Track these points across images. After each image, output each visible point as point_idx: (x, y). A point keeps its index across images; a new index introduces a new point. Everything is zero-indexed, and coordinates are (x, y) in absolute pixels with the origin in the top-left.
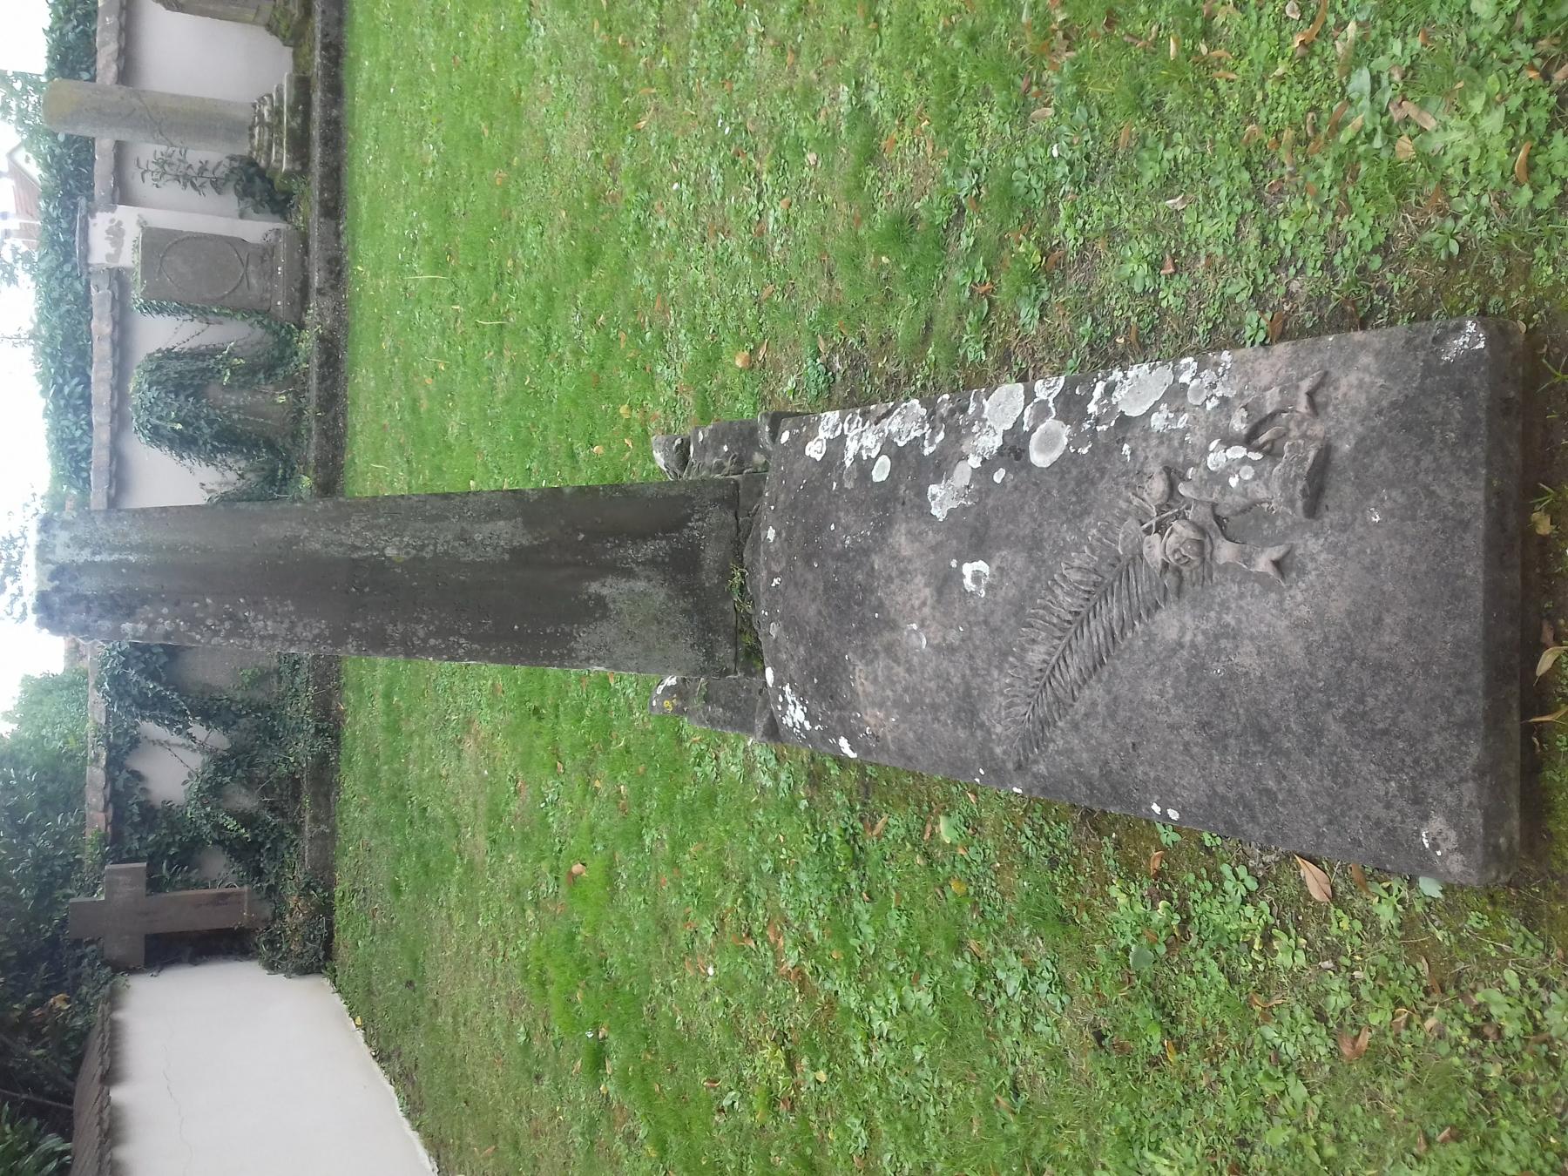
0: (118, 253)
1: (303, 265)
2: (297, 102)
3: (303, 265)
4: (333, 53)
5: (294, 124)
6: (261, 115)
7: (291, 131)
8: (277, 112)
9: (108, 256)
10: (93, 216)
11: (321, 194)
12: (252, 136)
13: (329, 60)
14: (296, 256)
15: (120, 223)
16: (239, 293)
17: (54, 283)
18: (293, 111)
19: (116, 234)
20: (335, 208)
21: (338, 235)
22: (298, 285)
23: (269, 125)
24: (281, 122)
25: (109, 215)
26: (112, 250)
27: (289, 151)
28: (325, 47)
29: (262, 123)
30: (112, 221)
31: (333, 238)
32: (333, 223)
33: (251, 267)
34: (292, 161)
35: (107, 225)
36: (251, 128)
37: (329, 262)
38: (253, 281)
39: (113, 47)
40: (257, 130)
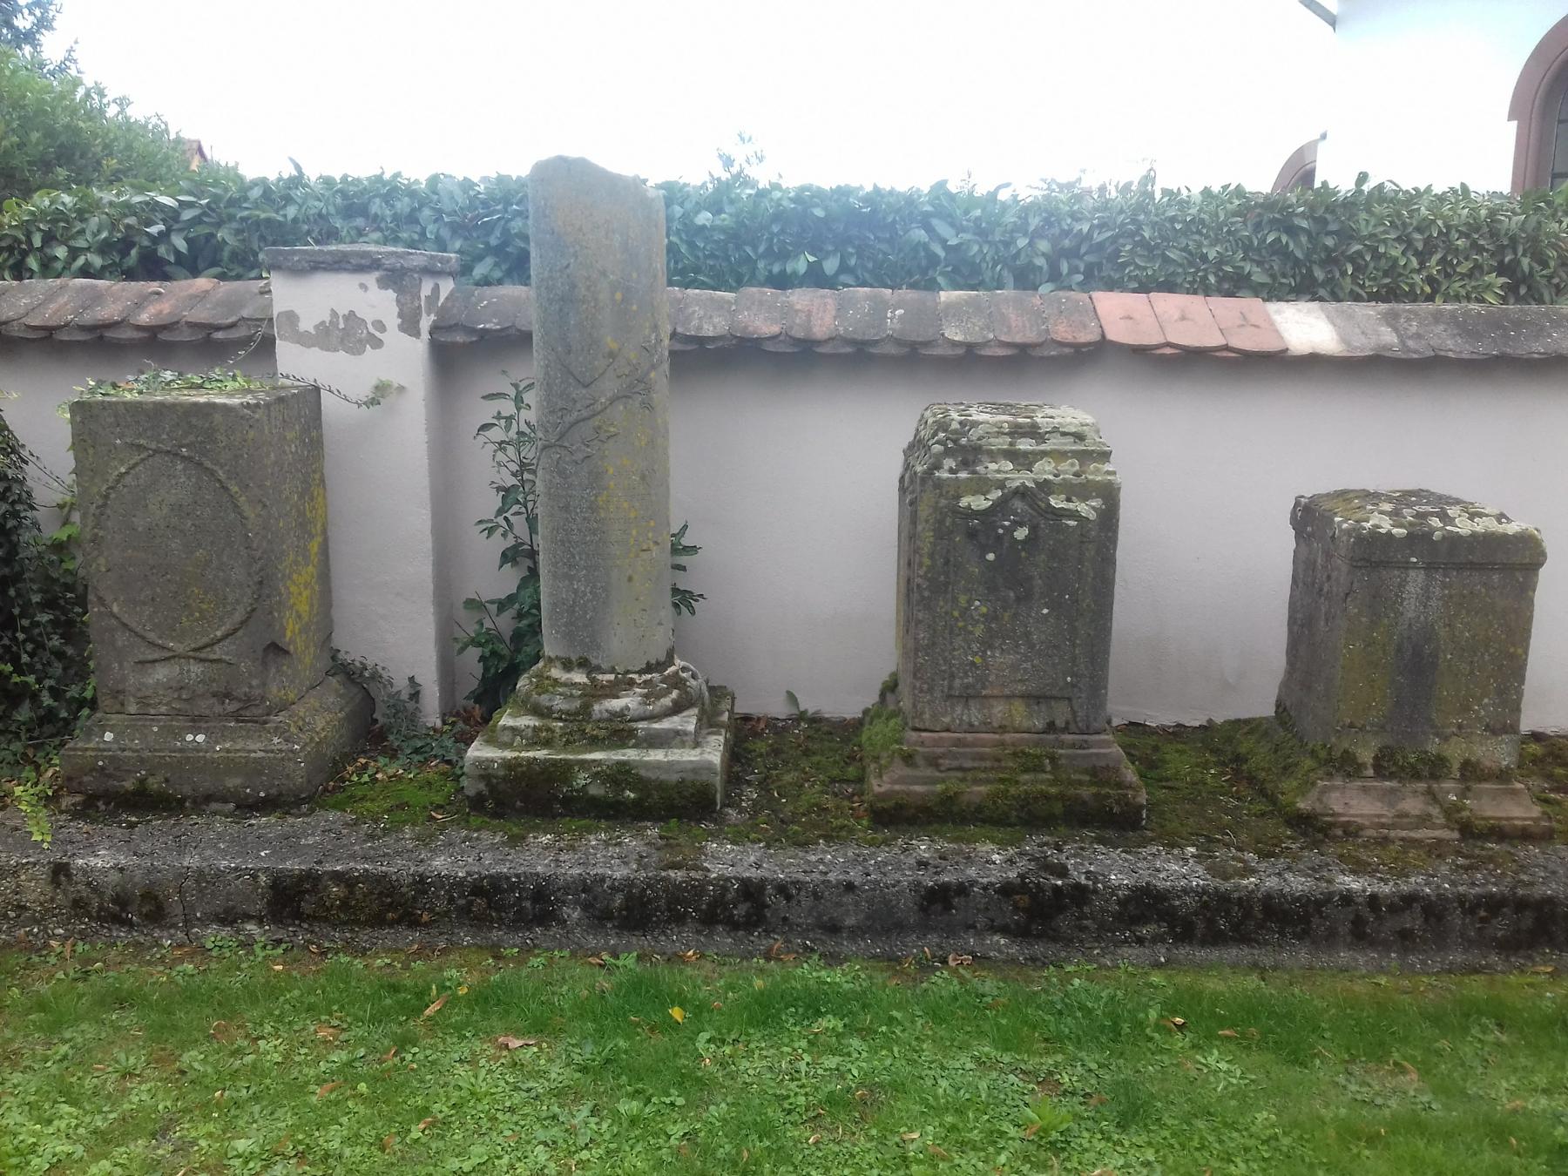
0: (304, 340)
1: (208, 798)
2: (641, 784)
3: (208, 798)
4: (740, 911)
5: (581, 779)
6: (613, 691)
7: (563, 771)
8: (620, 732)
9: (291, 317)
10: (383, 284)
11: (337, 877)
12: (567, 666)
13: (719, 902)
14: (233, 782)
15: (378, 344)
16: (121, 639)
17: (403, 205)
18: (621, 775)
19: (347, 334)
20: (298, 916)
21: (229, 918)
22: (154, 784)
23: (586, 710)
24: (595, 743)
25: (392, 320)
26: (307, 325)
27: (508, 765)
28: (751, 891)
29: (597, 692)
30: (380, 326)
31: (218, 904)
32: (259, 906)
33: (196, 669)
34: (484, 771)
35: (368, 315)
36: (584, 664)
37: (149, 896)
38: (161, 673)
39: (763, 325)
40: (579, 677)
